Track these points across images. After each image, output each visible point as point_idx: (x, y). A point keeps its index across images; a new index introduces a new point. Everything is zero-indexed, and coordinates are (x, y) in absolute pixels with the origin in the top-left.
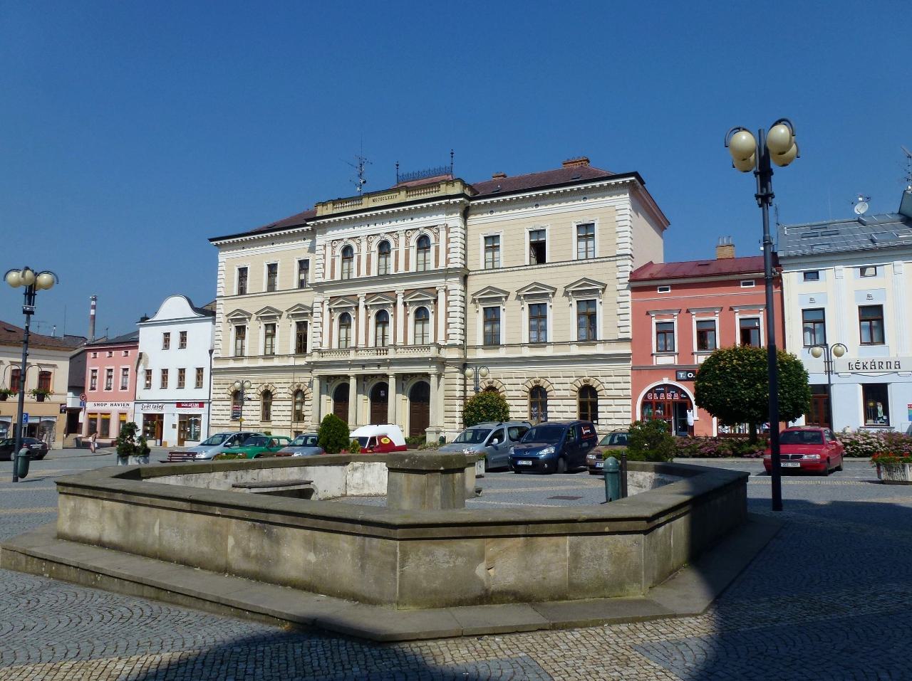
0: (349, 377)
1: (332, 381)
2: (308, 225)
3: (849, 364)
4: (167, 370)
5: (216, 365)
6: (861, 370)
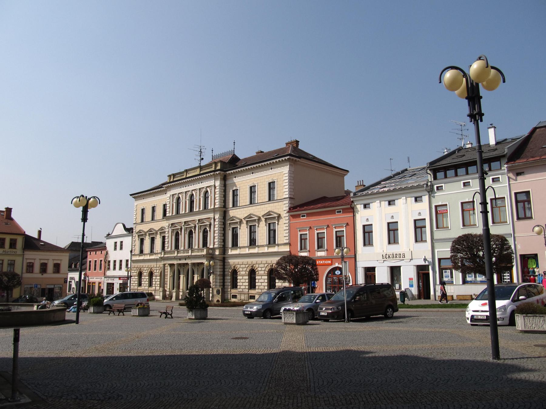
0: (175, 265)
1: (172, 267)
2: (163, 187)
3: (383, 255)
4: (116, 261)
5: (134, 258)
6: (388, 259)
